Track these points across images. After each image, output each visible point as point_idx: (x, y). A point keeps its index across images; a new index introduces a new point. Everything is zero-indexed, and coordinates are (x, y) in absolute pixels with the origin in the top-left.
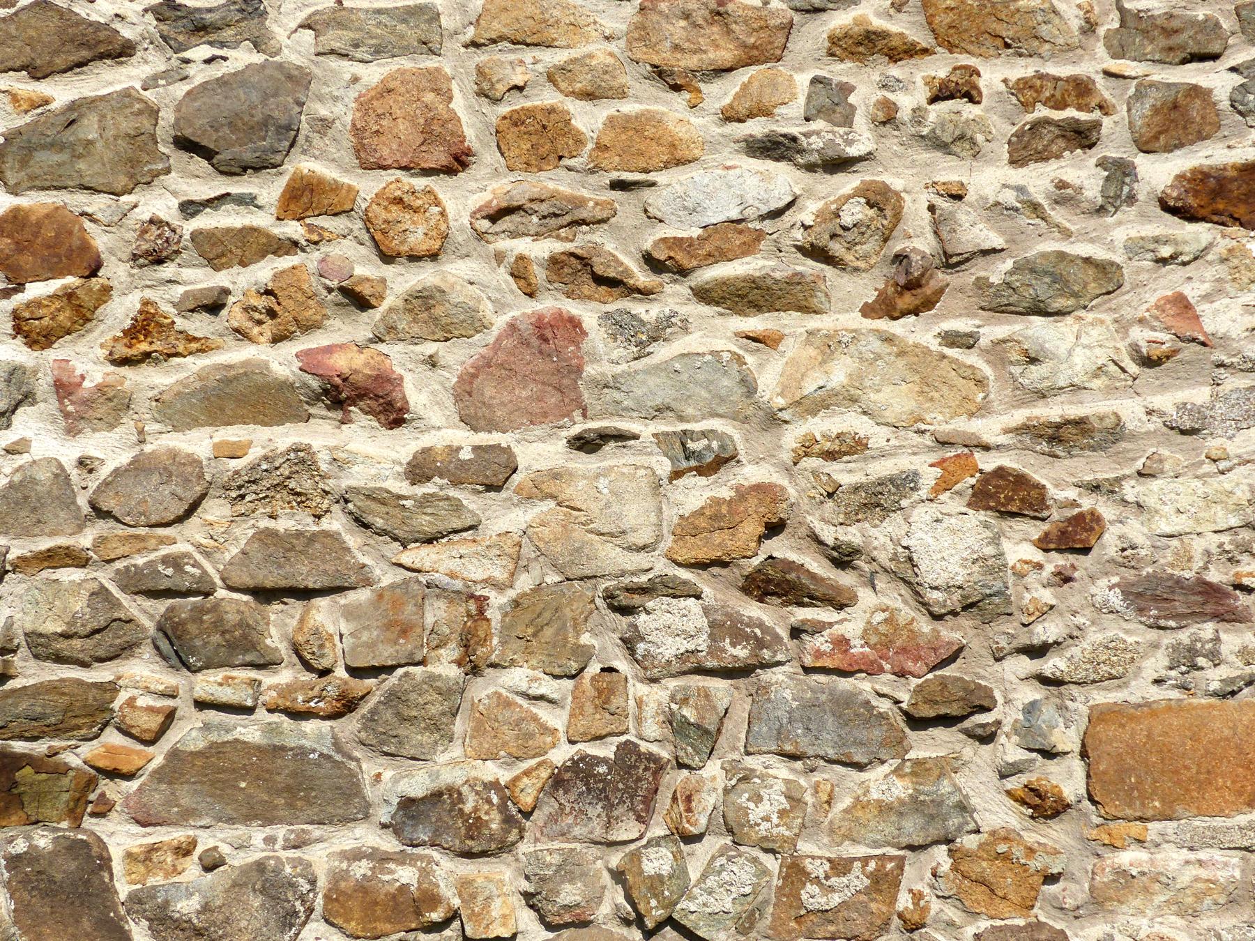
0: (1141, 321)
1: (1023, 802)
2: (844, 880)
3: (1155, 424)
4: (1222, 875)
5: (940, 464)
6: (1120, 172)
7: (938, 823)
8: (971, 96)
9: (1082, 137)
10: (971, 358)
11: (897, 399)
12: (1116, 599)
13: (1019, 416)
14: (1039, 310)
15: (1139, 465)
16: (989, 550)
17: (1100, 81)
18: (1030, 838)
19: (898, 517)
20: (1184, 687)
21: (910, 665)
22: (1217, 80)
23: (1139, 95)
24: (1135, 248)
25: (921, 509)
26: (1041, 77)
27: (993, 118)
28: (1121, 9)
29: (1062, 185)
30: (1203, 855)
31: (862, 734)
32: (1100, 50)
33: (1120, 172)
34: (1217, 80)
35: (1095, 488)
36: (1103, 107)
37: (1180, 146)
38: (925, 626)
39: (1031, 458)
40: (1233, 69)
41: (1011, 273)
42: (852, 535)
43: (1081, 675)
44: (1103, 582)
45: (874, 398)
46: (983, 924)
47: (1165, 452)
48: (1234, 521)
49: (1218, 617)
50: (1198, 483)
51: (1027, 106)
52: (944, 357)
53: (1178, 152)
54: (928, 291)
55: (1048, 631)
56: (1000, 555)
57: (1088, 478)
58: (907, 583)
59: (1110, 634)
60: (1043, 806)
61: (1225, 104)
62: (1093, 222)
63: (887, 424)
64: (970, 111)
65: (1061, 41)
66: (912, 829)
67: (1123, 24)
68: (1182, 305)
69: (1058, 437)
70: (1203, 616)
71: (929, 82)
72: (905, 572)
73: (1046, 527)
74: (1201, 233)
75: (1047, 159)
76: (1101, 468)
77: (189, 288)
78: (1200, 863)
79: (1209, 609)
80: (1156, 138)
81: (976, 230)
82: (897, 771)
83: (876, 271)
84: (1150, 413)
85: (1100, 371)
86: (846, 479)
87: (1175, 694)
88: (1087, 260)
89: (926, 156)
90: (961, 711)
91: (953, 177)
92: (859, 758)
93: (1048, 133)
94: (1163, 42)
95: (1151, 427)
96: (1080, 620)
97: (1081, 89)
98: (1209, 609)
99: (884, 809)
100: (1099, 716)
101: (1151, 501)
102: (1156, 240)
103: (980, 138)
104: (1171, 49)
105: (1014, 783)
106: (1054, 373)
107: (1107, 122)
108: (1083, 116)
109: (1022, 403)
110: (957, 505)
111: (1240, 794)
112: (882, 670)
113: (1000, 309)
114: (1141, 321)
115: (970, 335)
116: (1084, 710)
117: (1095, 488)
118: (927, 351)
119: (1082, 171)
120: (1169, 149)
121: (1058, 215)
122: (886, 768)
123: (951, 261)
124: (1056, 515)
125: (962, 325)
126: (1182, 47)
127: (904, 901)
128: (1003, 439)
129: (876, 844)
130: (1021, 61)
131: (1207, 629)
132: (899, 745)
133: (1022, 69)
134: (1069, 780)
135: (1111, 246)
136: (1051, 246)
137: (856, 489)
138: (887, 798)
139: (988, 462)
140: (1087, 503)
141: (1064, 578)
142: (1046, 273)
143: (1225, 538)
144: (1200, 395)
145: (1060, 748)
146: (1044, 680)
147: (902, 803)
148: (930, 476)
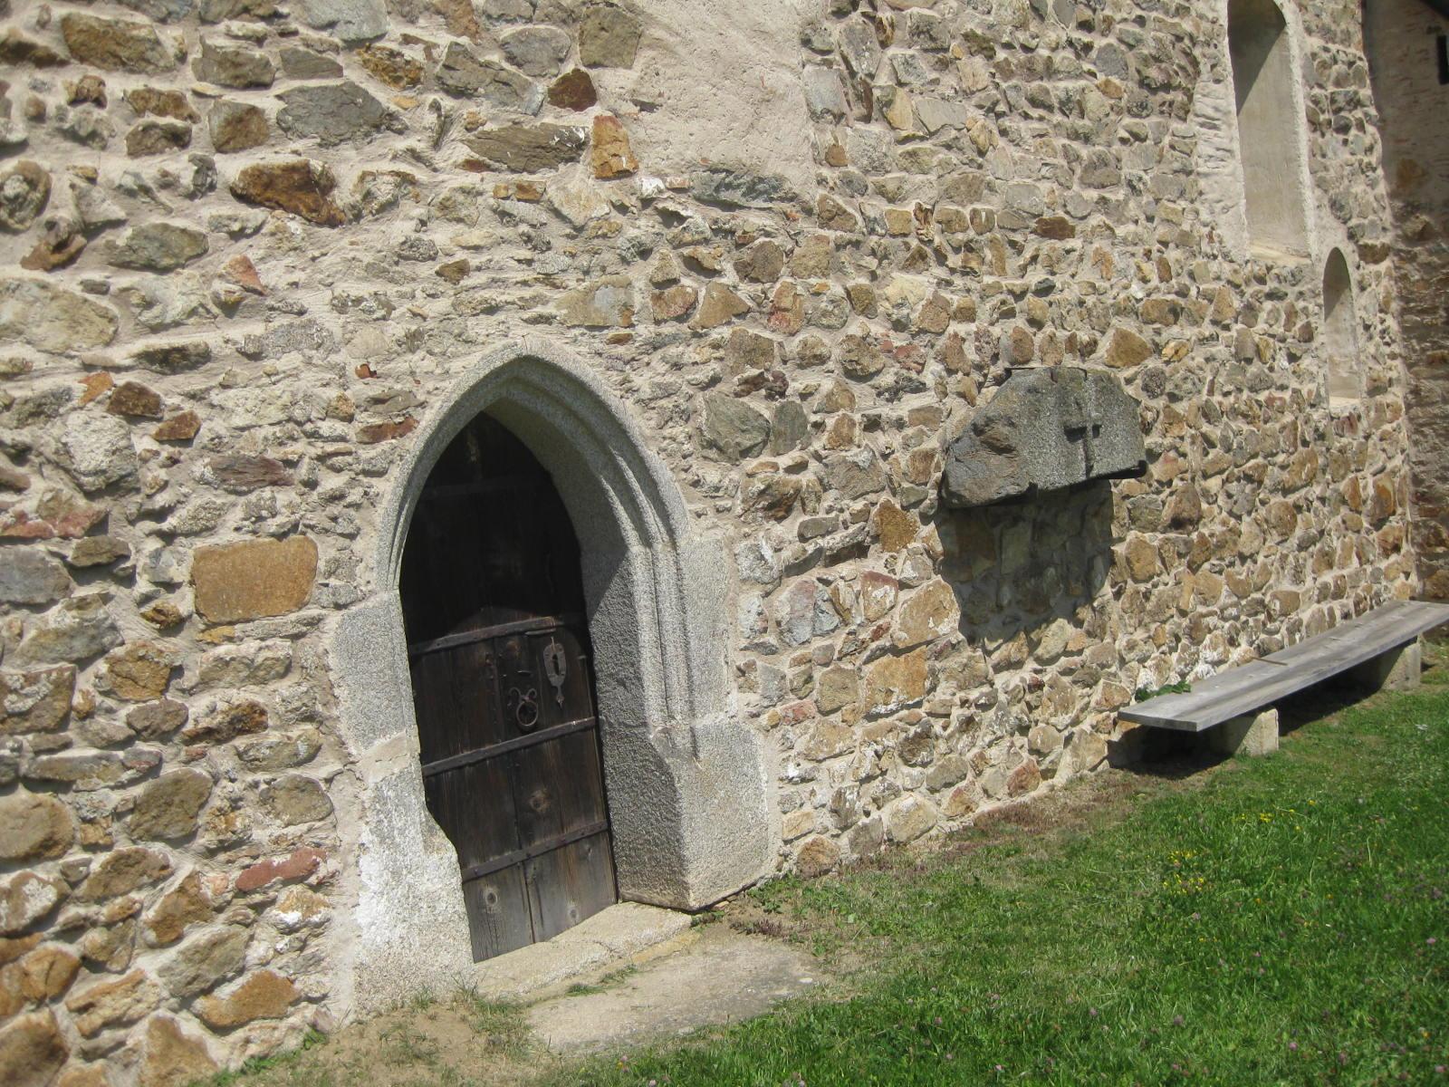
0: (221, 276)
1: (152, 620)
2: (35, 688)
3: (229, 350)
4: (281, 654)
5: (85, 381)
6: (204, 167)
7: (94, 643)
8: (99, 102)
9: (178, 139)
10: (104, 302)
11: (55, 336)
12: (209, 473)
13: (141, 345)
14: (150, 266)
15: (220, 378)
16: (123, 443)
17: (189, 96)
18: (160, 645)
19: (58, 421)
20: (254, 532)
21: (71, 530)
22: (268, 103)
23: (216, 109)
24: (217, 224)
25: (74, 416)
26: (150, 91)
27: (118, 123)
28: (203, 44)
29: (165, 174)
30: (269, 642)
31: (41, 583)
32: (188, 71)
33: (204, 167)
34: (268, 103)
35: (192, 396)
36: (192, 117)
37: (243, 148)
38: (81, 502)
39: (149, 375)
40: (279, 97)
41: (132, 238)
42: (24, 436)
43: (186, 528)
44: (200, 463)
45: (37, 332)
46: (131, 707)
47: (237, 369)
48: (282, 416)
49: (274, 483)
50: (258, 391)
51: (139, 112)
52: (86, 301)
53: (243, 154)
54: (72, 249)
55: (161, 500)
56: (130, 447)
57: (187, 389)
58: (67, 471)
59: (206, 499)
60: (171, 625)
61: (273, 121)
62: (187, 203)
63: (45, 351)
64: (98, 113)
65: (162, 63)
66: (80, 647)
67: (204, 55)
68: (248, 267)
69: (170, 361)
70: (262, 483)
71: (68, 86)
72: (62, 462)
73: (160, 425)
74: (255, 215)
75: (153, 154)
76: (193, 381)
77: (1067, 217)
78: (267, 647)
79: (268, 477)
80: (227, 142)
81: (105, 205)
82: (69, 608)
83: (31, 232)
84: (227, 342)
85: (193, 312)
86: (17, 394)
87: (249, 537)
88: (184, 231)
89: (68, 145)
90: (111, 568)
91: (89, 164)
92: (40, 599)
93: (156, 133)
94: (232, 72)
95: (228, 351)
96: (184, 490)
97: (175, 103)
98: (268, 477)
99: (60, 634)
100: (202, 556)
101: (230, 404)
102: (229, 218)
103: (106, 133)
104: (237, 77)
105: (147, 609)
106: (164, 312)
107: (195, 128)
108: (179, 123)
109: (140, 335)
110: (99, 411)
111: (290, 599)
112: (52, 535)
113: (126, 266)
114: (221, 276)
115: (103, 284)
116: (191, 552)
117: (192, 396)
118: (73, 296)
119: (180, 165)
120: (235, 150)
121: (163, 196)
122: (59, 606)
123: (91, 230)
124: (167, 416)
125: (96, 276)
126: (244, 76)
127: (77, 699)
128: (128, 362)
129: (55, 661)
130: (134, 77)
131: (267, 492)
132: (66, 589)
133: (136, 83)
134: (183, 602)
135: (199, 221)
136: (157, 219)
137: (26, 402)
138: (63, 626)
139: (121, 380)
140: (188, 406)
141: (173, 461)
142: (155, 239)
143: (277, 429)
144: (257, 328)
145: (177, 579)
146: (162, 535)
147: (72, 629)
148: (79, 388)
